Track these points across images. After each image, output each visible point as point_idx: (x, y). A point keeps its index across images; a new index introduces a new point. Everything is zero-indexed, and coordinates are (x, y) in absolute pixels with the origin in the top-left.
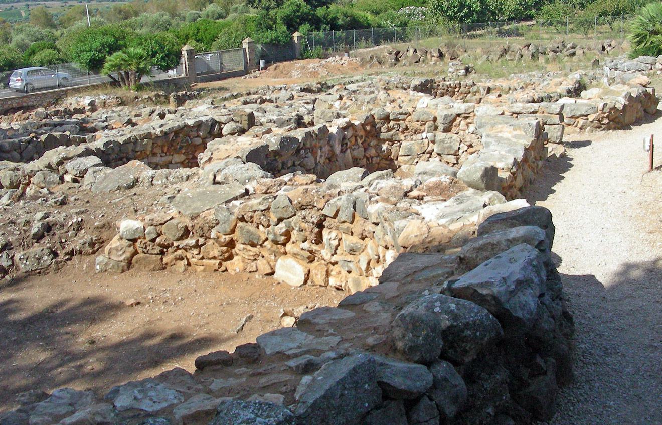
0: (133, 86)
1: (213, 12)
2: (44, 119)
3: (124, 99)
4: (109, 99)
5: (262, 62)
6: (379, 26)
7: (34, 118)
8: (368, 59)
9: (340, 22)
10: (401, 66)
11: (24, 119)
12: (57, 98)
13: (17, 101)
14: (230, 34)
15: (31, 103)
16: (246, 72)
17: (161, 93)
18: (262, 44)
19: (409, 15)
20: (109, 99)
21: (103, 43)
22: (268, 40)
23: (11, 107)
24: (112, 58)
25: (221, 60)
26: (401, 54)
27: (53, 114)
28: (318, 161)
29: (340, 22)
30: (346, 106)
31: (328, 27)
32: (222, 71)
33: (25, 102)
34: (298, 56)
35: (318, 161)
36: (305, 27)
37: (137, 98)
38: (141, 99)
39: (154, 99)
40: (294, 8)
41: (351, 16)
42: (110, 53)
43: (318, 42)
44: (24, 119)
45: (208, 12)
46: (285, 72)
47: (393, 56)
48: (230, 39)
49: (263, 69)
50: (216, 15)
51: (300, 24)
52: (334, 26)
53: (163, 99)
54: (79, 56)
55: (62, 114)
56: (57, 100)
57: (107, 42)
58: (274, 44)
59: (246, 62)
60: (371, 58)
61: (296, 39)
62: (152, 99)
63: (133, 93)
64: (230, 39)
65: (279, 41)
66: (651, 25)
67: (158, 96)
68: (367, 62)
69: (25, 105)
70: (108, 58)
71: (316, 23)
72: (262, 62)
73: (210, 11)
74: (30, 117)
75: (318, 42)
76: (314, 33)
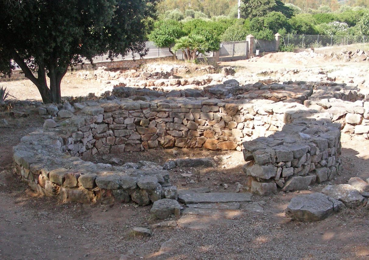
0: (194, 61)
1: (177, 14)
2: (149, 77)
3: (190, 68)
4: (180, 67)
5: (257, 52)
6: (324, 34)
7: (143, 76)
8: (330, 55)
9: (303, 29)
10: (353, 62)
11: (136, 77)
12: (140, 64)
13: (116, 64)
14: (233, 31)
15: (125, 66)
16: (247, 57)
17: (212, 67)
18: (258, 39)
19: (336, 28)
20: (180, 67)
21: (174, 30)
22: (262, 37)
23: (113, 67)
24: (180, 40)
25: (234, 48)
26: (352, 54)
27: (155, 74)
28: (187, 205)
29: (303, 29)
30: (152, 141)
31: (296, 32)
32: (233, 55)
33: (121, 65)
34: (277, 49)
35: (187, 205)
36: (283, 31)
37: (197, 69)
38: (199, 70)
39: (208, 70)
40: (276, 18)
41: (309, 26)
42: (178, 37)
43: (291, 42)
44: (136, 77)
45: (173, 14)
46: (277, 60)
47: (347, 55)
48: (233, 34)
49: (257, 56)
50: (179, 17)
51: (278, 28)
52: (300, 32)
53: (213, 70)
54: (156, 38)
55: (160, 75)
56: (140, 65)
57: (176, 30)
58: (264, 40)
59: (248, 51)
60: (332, 55)
61: (277, 38)
62: (207, 70)
63: (194, 65)
64: (233, 34)
65: (268, 38)
66: (297, 252)
67: (210, 68)
68: (329, 57)
69: (121, 67)
70: (177, 40)
71: (289, 29)
72: (257, 52)
73: (175, 14)
74: (140, 75)
75: (291, 42)
76: (288, 35)
